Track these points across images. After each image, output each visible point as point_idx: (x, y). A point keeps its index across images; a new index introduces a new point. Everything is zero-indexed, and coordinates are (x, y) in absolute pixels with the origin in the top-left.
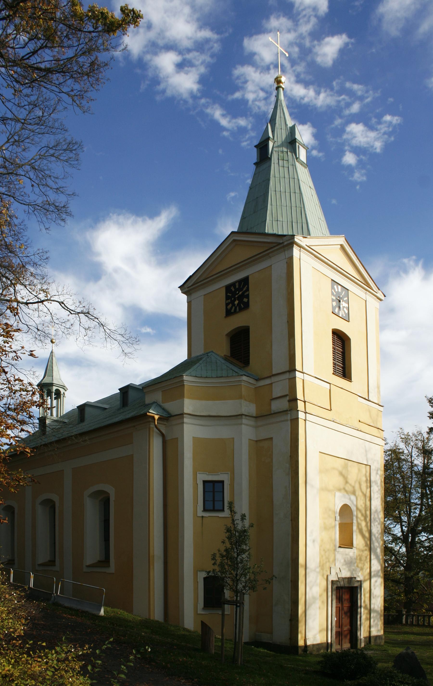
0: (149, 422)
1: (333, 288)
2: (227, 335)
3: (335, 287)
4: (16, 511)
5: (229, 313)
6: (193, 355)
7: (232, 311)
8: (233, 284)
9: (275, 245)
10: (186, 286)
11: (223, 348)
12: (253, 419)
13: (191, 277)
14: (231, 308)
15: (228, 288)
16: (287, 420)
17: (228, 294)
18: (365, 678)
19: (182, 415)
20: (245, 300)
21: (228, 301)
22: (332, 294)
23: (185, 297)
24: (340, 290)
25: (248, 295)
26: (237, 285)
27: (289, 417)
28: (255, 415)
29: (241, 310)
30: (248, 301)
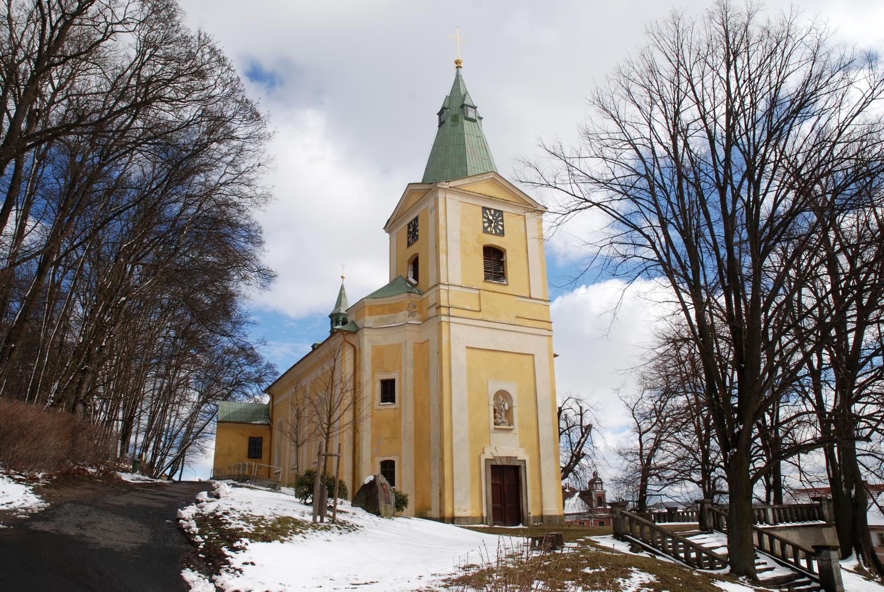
5: (409, 245)
23: (388, 235)
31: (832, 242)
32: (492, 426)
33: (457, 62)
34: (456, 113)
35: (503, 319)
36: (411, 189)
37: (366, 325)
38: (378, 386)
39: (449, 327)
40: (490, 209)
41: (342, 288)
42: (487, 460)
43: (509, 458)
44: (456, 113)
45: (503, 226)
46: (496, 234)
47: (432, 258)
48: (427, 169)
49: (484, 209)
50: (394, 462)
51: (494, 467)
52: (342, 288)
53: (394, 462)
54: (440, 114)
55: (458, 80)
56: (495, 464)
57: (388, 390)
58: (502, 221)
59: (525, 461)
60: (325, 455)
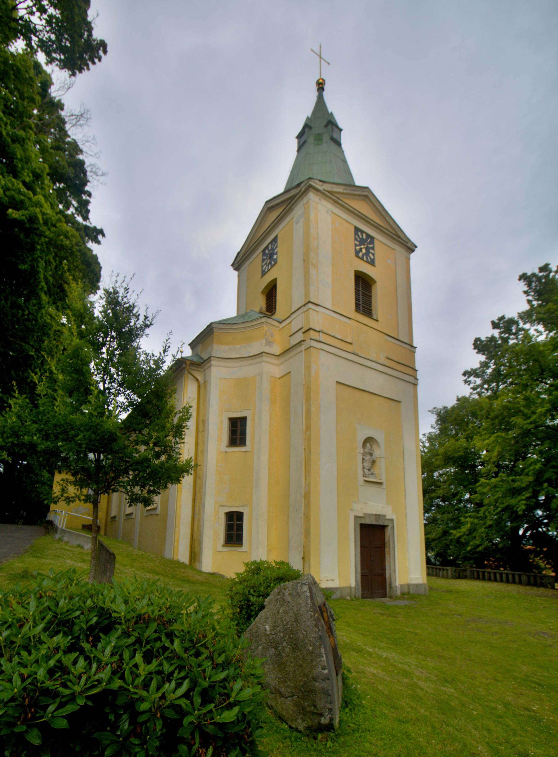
2: (262, 292)
3: (359, 233)
8: (267, 247)
10: (236, 262)
11: (261, 302)
13: (239, 253)
15: (264, 251)
16: (301, 351)
22: (356, 239)
23: (236, 273)
27: (303, 348)
32: (361, 479)
35: (373, 356)
36: (271, 206)
37: (214, 355)
38: (226, 426)
40: (362, 232)
42: (356, 517)
43: (378, 516)
45: (373, 255)
46: (367, 262)
48: (292, 172)
49: (357, 230)
50: (242, 513)
51: (383, 527)
53: (242, 513)
55: (320, 103)
56: (364, 522)
57: (237, 431)
58: (373, 248)
59: (392, 520)
60: (331, 719)
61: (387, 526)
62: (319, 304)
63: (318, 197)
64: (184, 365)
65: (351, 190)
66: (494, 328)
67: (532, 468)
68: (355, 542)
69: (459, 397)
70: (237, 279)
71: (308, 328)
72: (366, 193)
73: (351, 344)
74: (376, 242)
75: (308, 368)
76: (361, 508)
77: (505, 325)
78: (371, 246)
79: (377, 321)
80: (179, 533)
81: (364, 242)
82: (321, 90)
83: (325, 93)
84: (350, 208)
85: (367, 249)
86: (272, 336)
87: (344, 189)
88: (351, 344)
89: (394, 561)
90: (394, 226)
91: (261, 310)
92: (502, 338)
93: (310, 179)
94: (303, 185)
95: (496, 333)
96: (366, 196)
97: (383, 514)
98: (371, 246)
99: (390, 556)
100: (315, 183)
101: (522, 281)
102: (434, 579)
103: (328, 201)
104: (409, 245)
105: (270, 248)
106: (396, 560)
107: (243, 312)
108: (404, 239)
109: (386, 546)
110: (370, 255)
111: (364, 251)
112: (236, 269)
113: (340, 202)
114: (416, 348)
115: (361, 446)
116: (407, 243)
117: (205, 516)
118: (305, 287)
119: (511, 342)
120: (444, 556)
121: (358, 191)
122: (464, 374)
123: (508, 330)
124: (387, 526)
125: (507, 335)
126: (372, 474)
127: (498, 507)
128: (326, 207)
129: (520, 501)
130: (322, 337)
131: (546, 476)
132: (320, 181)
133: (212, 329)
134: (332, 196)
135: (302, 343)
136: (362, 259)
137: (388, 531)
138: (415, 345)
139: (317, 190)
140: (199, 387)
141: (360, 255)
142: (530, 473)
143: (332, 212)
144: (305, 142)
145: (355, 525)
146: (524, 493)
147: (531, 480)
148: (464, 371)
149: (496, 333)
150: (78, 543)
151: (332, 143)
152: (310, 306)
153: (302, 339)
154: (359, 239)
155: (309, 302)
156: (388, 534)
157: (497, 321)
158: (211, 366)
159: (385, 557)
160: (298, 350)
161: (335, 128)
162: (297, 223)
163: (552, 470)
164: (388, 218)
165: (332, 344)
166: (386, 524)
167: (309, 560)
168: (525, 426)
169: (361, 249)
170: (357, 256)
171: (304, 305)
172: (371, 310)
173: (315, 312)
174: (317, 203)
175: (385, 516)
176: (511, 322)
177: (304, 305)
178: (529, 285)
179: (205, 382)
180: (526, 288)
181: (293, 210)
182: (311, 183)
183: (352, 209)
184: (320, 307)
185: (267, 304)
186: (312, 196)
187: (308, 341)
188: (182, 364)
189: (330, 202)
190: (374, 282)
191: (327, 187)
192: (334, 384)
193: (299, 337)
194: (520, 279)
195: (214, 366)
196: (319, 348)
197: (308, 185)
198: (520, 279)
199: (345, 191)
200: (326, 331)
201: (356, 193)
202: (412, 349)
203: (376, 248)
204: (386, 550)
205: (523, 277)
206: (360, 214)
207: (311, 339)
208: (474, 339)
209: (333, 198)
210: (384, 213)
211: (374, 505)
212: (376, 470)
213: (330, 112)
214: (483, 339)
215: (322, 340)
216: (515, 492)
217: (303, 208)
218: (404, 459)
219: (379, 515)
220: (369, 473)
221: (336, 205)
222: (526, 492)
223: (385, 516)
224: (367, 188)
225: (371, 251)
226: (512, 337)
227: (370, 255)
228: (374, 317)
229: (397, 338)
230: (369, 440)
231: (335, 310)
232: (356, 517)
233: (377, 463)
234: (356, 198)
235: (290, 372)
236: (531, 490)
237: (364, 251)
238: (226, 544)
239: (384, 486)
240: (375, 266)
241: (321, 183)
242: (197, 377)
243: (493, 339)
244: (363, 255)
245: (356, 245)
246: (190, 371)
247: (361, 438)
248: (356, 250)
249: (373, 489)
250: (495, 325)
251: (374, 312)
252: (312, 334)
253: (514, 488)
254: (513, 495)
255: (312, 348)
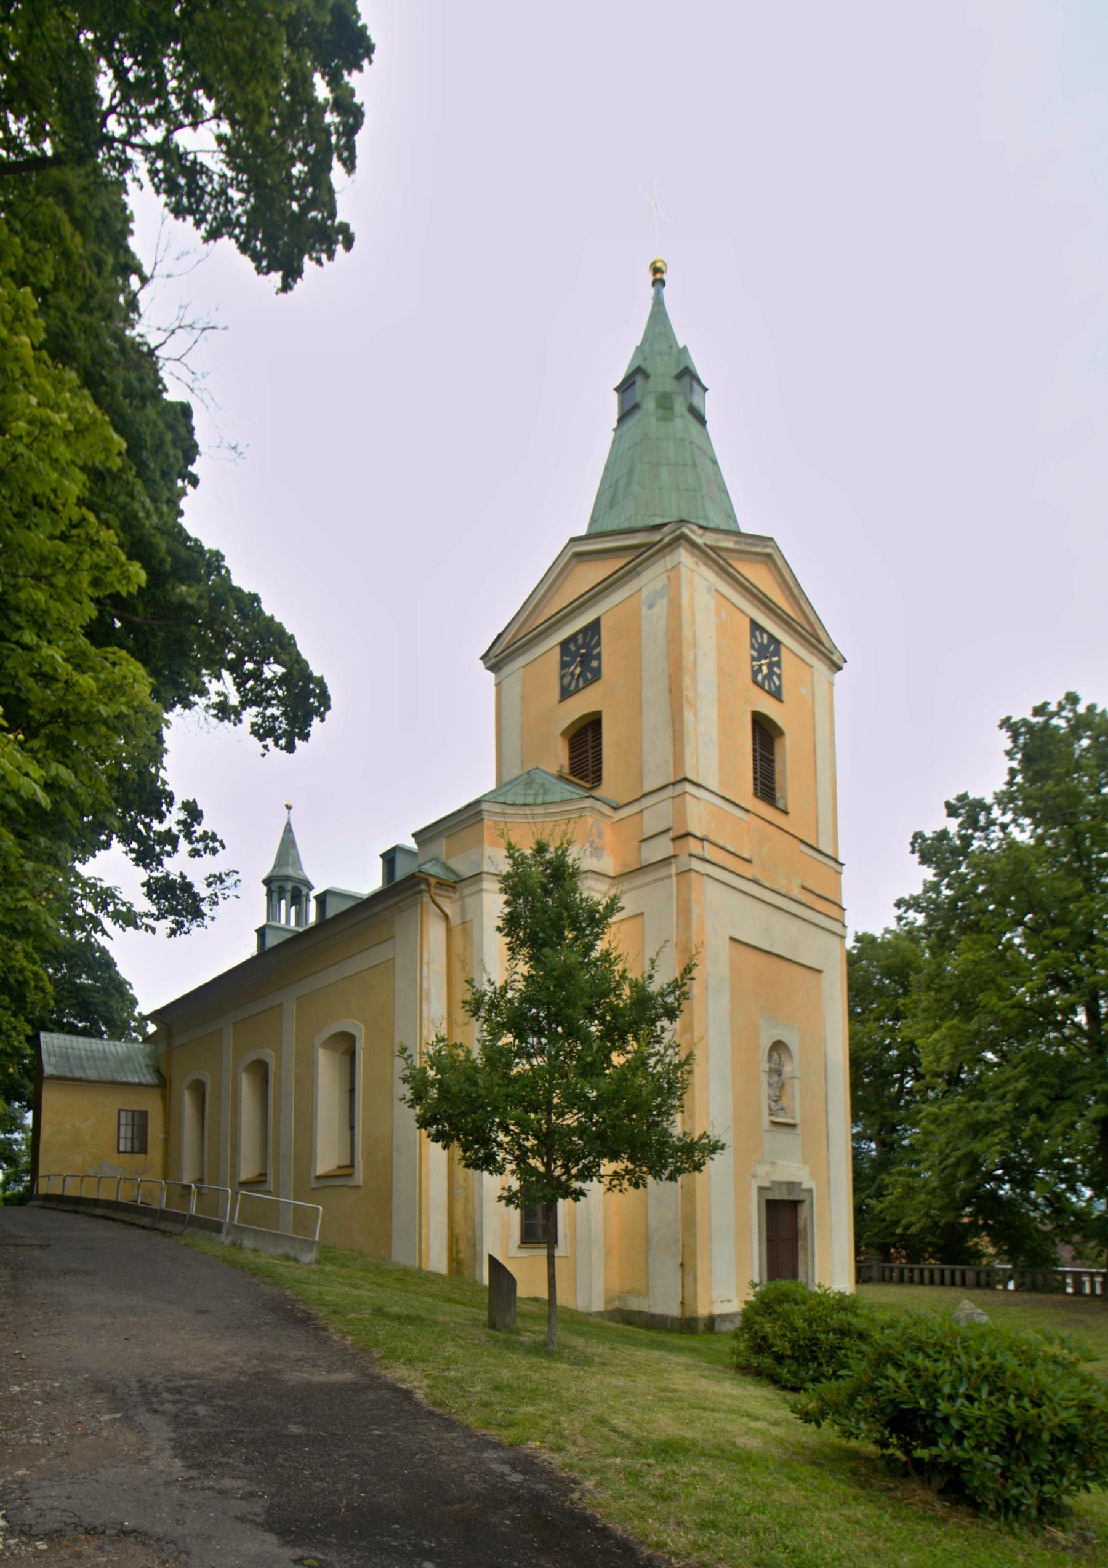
0: (421, 892)
1: (753, 635)
2: (563, 734)
3: (757, 634)
4: (208, 1089)
5: (566, 693)
6: (506, 779)
7: (572, 688)
8: (572, 638)
9: (643, 550)
10: (492, 654)
11: (559, 756)
12: (610, 881)
13: (500, 636)
14: (570, 683)
15: (564, 645)
16: (670, 876)
17: (565, 658)
18: (1060, 1535)
19: (478, 876)
20: (594, 664)
21: (564, 672)
22: (752, 647)
23: (491, 676)
24: (765, 642)
25: (599, 654)
26: (580, 637)
27: (673, 870)
28: (612, 875)
29: (588, 684)
30: (600, 665)
31: (629, 1056)
32: (766, 1119)
33: (656, 270)
34: (659, 391)
35: (781, 885)
39: (132, 1147)
40: (763, 630)
41: (288, 829)
42: (761, 1189)
43: (791, 1185)
44: (659, 391)
45: (779, 677)
46: (769, 693)
47: (655, 717)
49: (755, 626)
51: (795, 1204)
52: (288, 829)
54: (625, 388)
55: (659, 314)
58: (778, 664)
59: (810, 1191)
61: (802, 1202)
62: (700, 782)
63: (694, 559)
64: (423, 887)
65: (747, 544)
66: (949, 815)
67: (1011, 1087)
68: (760, 1232)
69: (860, 934)
70: (493, 690)
71: (683, 832)
72: (768, 550)
73: (749, 861)
74: (783, 650)
75: (685, 911)
76: (767, 1173)
77: (968, 810)
78: (775, 659)
79: (786, 813)
80: (428, 1224)
81: (767, 649)
82: (658, 285)
83: (666, 292)
84: (746, 583)
85: (770, 666)
86: (600, 836)
87: (736, 543)
88: (749, 861)
89: (813, 1262)
90: (813, 619)
91: (560, 771)
92: (963, 838)
93: (682, 522)
94: (665, 529)
95: (953, 826)
96: (769, 556)
97: (797, 1180)
98: (775, 659)
99: (806, 1254)
100: (692, 531)
101: (1004, 730)
102: (860, 1286)
103: (710, 568)
104: (834, 658)
105: (580, 642)
106: (816, 1259)
107: (513, 771)
108: (827, 645)
109: (800, 1237)
110: (775, 678)
111: (765, 670)
112: (494, 668)
113: (731, 570)
114: (843, 865)
115: (766, 1059)
116: (832, 653)
117: (485, 1192)
118: (675, 746)
119: (976, 844)
120: (880, 1248)
121: (756, 546)
122: (898, 905)
123: (972, 822)
124: (802, 1202)
125: (970, 831)
126: (782, 1109)
127: (948, 1156)
128: (705, 579)
129: (989, 1147)
130: (709, 852)
131: (1032, 1101)
132: (701, 527)
133: (480, 812)
134: (717, 558)
135: (673, 860)
136: (761, 687)
137: (803, 1211)
138: (841, 860)
139: (693, 544)
140: (449, 930)
141: (760, 678)
142: (1009, 1096)
143: (717, 591)
144: (636, 407)
145: (759, 1202)
146: (995, 1132)
147: (1009, 1109)
148: (898, 898)
149: (953, 826)
150: (280, 1251)
151: (689, 417)
152: (689, 788)
153: (672, 854)
154: (756, 646)
155: (686, 779)
156: (803, 1216)
157: (953, 802)
158: (481, 890)
159: (797, 1255)
160: (663, 872)
161: (696, 386)
162: (651, 607)
163: (1041, 1091)
164: (802, 603)
165: (722, 864)
166: (801, 1198)
167: (695, 1266)
168: (1003, 1012)
169: (761, 666)
170: (755, 682)
171: (674, 784)
172: (773, 789)
173: (694, 800)
174: (693, 571)
175: (800, 1184)
176: (980, 806)
177: (674, 784)
178: (1015, 738)
179: (464, 923)
180: (1009, 745)
181: (639, 574)
182: (685, 530)
183: (749, 585)
184: (702, 790)
185: (571, 759)
186: (684, 556)
187: (683, 858)
188: (419, 883)
189: (713, 570)
190: (780, 733)
191: (709, 539)
192: (727, 940)
193: (662, 848)
194: (1001, 727)
195: (487, 891)
196: (702, 871)
197: (678, 533)
198: (1001, 727)
199: (737, 547)
200: (712, 838)
201: (754, 549)
202: (837, 867)
203: (783, 664)
204: (800, 1243)
205: (1006, 723)
206: (760, 595)
207: (691, 855)
208: (912, 834)
209: (713, 557)
210: (796, 592)
211: (790, 1168)
212: (785, 1101)
213: (681, 346)
214: (928, 834)
215: (708, 857)
216: (978, 1130)
217: (664, 576)
218: (826, 1079)
219: (793, 1183)
220: (777, 1107)
221: (724, 576)
222: (1000, 1130)
223: (800, 1184)
224: (771, 539)
225: (776, 670)
226: (977, 834)
227: (775, 678)
228: (780, 804)
229: (815, 845)
230: (778, 1046)
231: (727, 796)
232: (761, 1189)
233: (787, 1088)
234: (744, 557)
235: (642, 914)
236: (1008, 1127)
237: (765, 670)
238: (522, 1242)
239: (799, 1130)
240: (782, 702)
241: (701, 532)
242: (448, 911)
243: (943, 835)
244: (764, 677)
245: (753, 659)
246: (437, 898)
247: (766, 1043)
248: (753, 667)
249: (783, 1135)
250: (952, 810)
251: (778, 795)
252: (694, 846)
253: (978, 1123)
254: (975, 1136)
255: (693, 874)
